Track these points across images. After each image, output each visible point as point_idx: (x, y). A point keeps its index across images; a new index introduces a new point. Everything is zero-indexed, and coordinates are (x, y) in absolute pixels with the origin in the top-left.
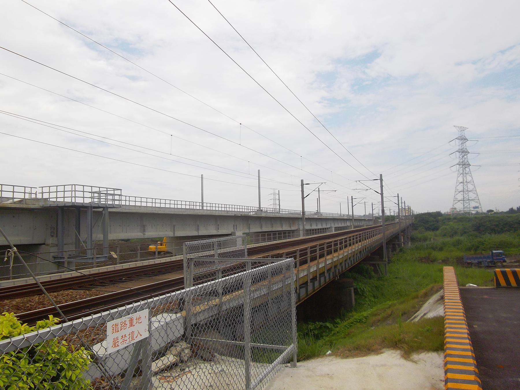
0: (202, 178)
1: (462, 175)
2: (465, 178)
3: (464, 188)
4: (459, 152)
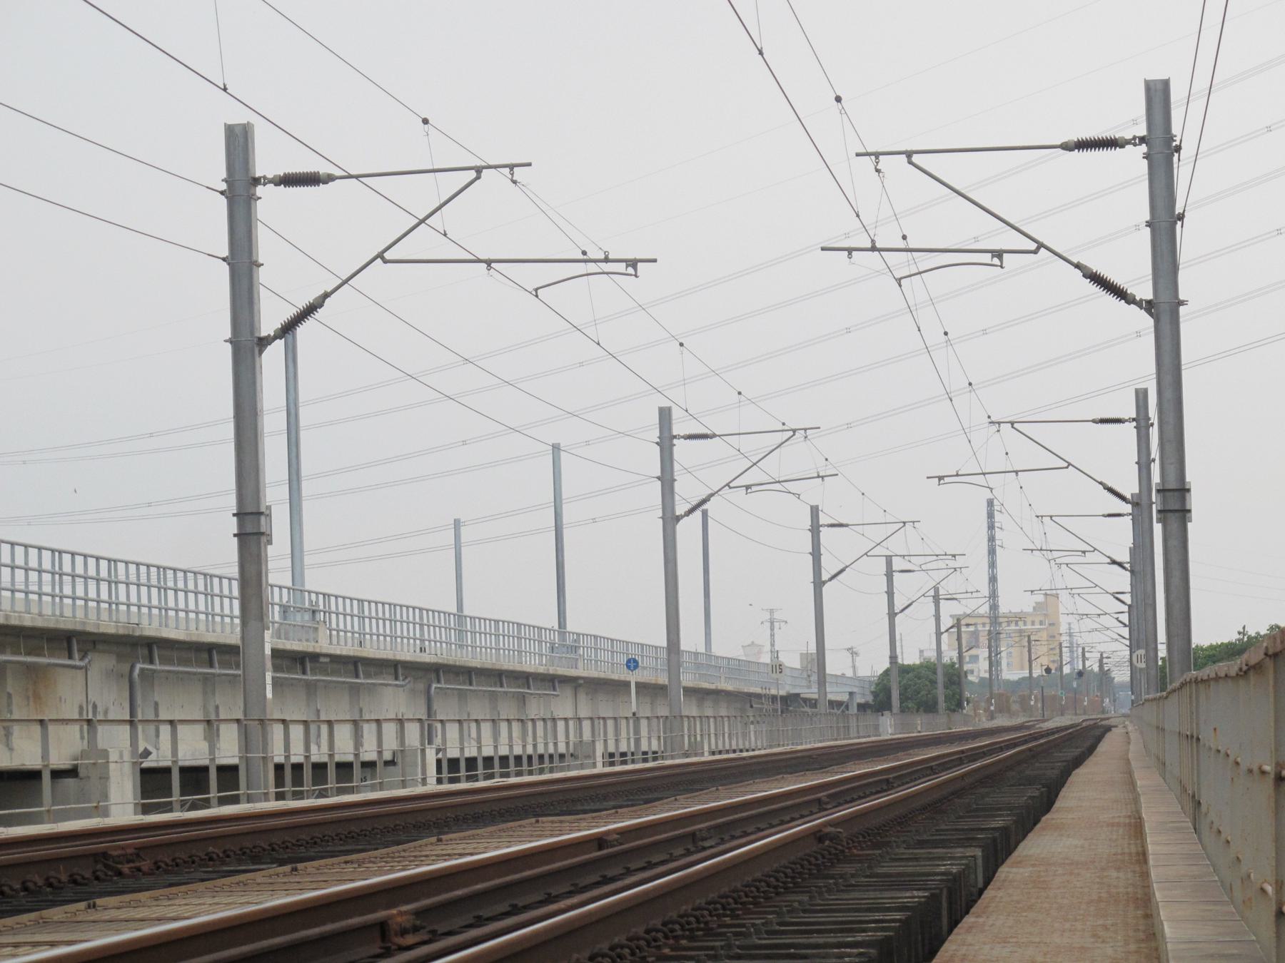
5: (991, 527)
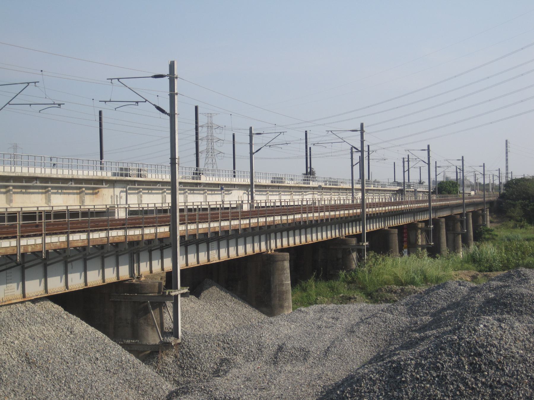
5: (507, 147)
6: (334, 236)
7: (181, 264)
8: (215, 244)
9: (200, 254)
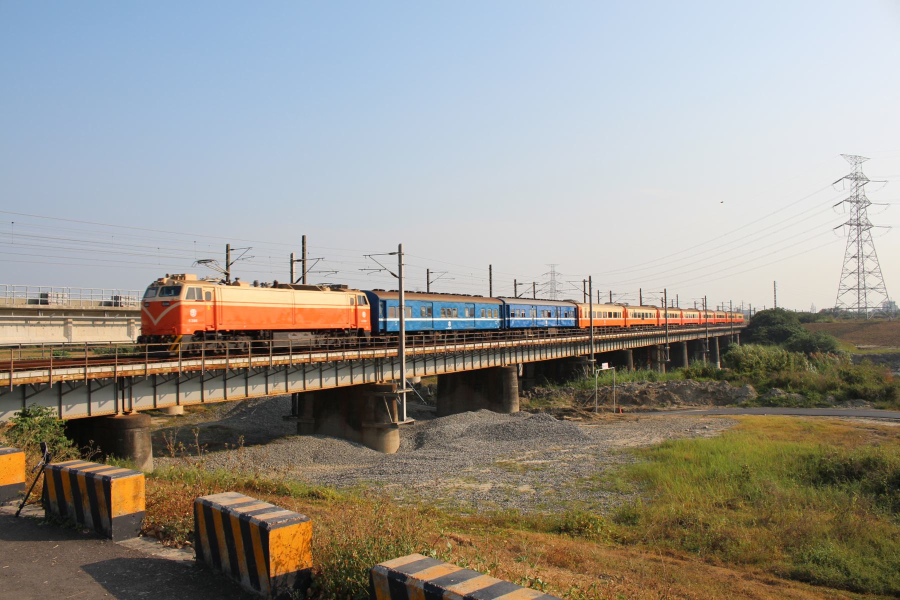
0: (490, 269)
1: (855, 244)
2: (862, 297)
3: (861, 298)
4: (851, 202)
6: (618, 348)
7: (594, 351)
8: (544, 351)
9: (92, 404)
